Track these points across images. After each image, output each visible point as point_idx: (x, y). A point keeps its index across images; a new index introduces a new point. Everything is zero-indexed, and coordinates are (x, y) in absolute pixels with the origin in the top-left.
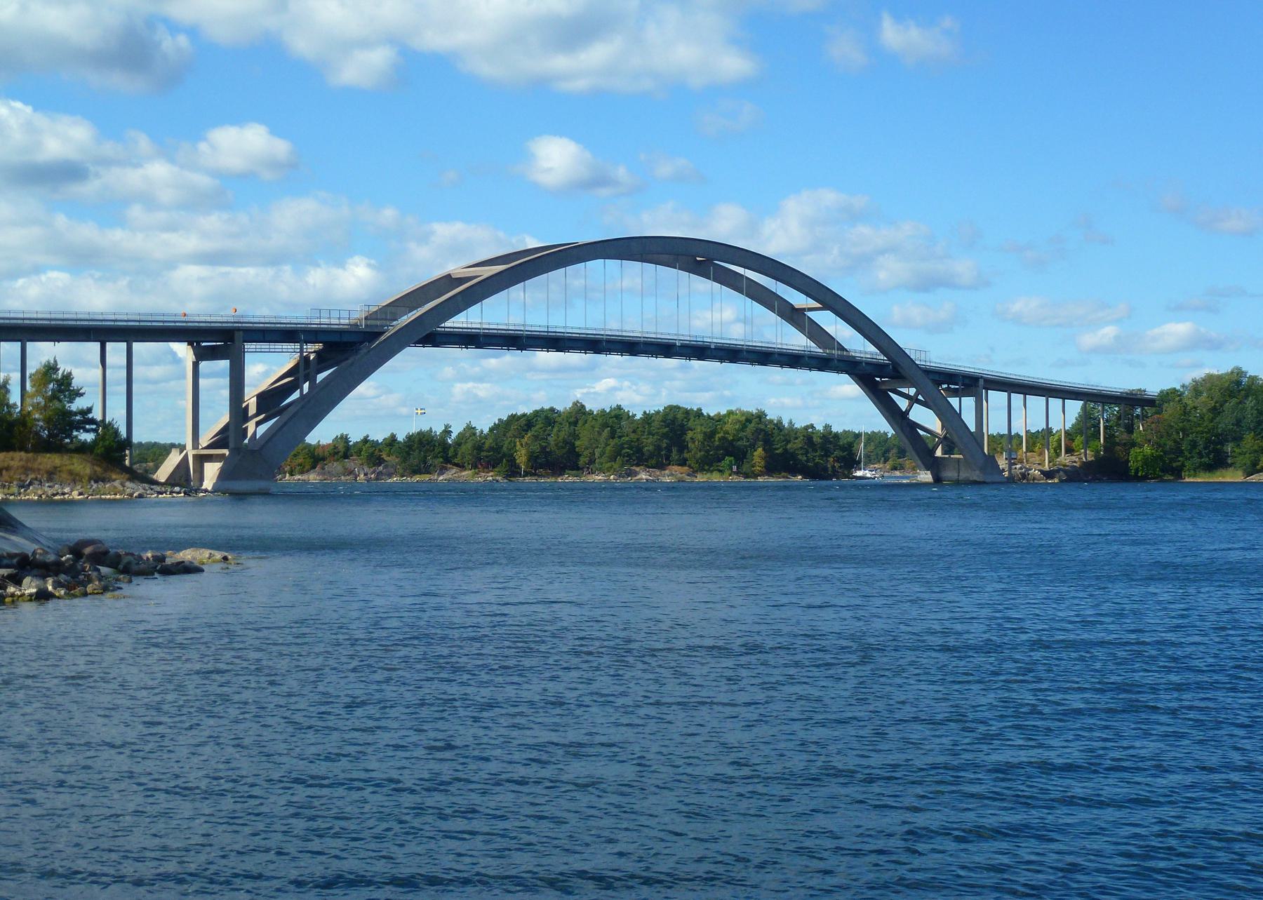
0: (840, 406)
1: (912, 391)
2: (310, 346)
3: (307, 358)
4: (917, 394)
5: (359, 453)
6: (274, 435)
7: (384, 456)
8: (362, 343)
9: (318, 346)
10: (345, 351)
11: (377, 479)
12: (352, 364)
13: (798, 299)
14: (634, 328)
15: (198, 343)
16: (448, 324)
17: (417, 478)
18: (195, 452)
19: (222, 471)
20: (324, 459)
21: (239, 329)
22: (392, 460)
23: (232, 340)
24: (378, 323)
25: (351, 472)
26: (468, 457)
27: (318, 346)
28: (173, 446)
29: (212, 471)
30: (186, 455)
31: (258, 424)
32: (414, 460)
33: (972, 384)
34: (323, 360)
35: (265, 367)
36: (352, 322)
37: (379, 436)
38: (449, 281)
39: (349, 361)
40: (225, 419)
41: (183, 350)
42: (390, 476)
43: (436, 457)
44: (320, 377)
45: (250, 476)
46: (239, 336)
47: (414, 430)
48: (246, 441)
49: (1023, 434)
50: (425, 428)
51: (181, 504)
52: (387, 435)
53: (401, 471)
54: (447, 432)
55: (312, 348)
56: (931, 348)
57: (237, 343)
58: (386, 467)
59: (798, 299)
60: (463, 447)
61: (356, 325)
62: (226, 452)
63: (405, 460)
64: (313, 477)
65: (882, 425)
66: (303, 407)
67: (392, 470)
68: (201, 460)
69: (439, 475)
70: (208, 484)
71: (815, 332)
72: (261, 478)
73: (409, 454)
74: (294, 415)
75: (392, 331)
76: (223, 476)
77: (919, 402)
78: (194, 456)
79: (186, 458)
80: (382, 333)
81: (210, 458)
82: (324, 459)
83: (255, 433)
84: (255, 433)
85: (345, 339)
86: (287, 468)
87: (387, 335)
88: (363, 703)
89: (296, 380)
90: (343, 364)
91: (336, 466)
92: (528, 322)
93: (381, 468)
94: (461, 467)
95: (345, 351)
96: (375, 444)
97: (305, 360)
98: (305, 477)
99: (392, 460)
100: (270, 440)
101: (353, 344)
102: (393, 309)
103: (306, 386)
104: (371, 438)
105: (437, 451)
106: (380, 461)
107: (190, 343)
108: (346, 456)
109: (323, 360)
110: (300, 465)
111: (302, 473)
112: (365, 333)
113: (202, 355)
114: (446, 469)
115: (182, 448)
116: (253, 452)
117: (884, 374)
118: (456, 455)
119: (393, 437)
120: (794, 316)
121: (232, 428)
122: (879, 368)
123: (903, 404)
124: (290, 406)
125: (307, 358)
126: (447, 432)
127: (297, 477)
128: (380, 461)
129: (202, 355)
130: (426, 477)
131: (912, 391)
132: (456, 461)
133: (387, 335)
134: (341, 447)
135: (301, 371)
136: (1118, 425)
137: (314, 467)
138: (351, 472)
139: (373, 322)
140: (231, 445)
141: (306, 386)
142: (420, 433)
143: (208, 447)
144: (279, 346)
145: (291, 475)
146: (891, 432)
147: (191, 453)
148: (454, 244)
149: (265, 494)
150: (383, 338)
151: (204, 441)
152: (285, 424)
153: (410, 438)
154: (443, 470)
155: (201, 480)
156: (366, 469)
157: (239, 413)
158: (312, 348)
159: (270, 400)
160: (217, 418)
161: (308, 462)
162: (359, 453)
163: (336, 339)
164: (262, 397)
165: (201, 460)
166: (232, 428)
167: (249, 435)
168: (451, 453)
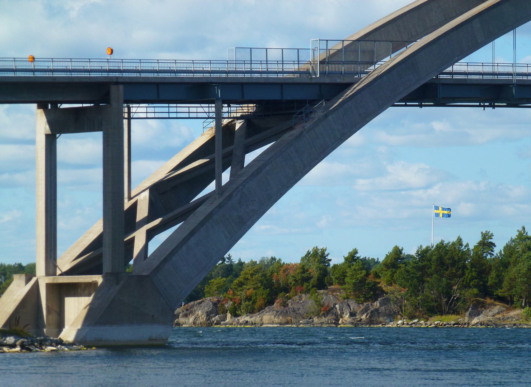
2: (234, 108)
3: (230, 127)
5: (341, 281)
6: (173, 253)
7: (383, 285)
8: (313, 102)
9: (249, 108)
10: (288, 116)
11: (370, 322)
12: (299, 137)
15: (55, 104)
16: (458, 67)
17: (435, 321)
18: (50, 280)
19: (92, 310)
20: (286, 289)
21: (117, 82)
22: (394, 291)
23: (106, 98)
24: (343, 68)
25: (329, 311)
26: (520, 288)
27: (249, 108)
28: (19, 269)
29: (76, 308)
30: (36, 285)
31: (150, 234)
32: (430, 292)
34: (255, 130)
35: (164, 141)
36: (303, 67)
37: (376, 250)
39: (295, 132)
40: (97, 228)
41: (32, 120)
42: (392, 316)
43: (467, 286)
44: (250, 158)
45: (138, 317)
46: (117, 92)
47: (431, 240)
48: (131, 262)
50: (450, 238)
51: (343, 344)
52: (389, 249)
53: (409, 309)
54: (486, 243)
55: (236, 113)
57: (114, 104)
58: (386, 301)
60: (513, 271)
61: (307, 72)
62: (99, 279)
63: (416, 291)
64: (268, 319)
66: (220, 206)
67: (394, 307)
68: (60, 292)
69: (472, 316)
70: (68, 334)
72: (153, 321)
73: (421, 281)
74: (210, 216)
75: (365, 80)
76: (92, 318)
78: (49, 286)
79: (36, 287)
80: (349, 85)
81: (73, 290)
82: (286, 289)
83: (146, 247)
84: (145, 248)
85: (290, 95)
86: (229, 305)
87: (357, 87)
89: (211, 162)
90: (287, 136)
91: (306, 301)
92: (521, 60)
93: (377, 304)
94: (508, 302)
95: (288, 116)
96: (367, 265)
97: (225, 133)
98: (255, 318)
99: (394, 291)
100: (165, 260)
101: (301, 103)
102: (368, 46)
103: (226, 176)
104: (361, 255)
105: (468, 275)
106: (375, 292)
107: (42, 105)
108: (321, 284)
109: (255, 130)
110: (248, 298)
111: (251, 311)
112: (320, 85)
113: (62, 124)
114: (484, 306)
115: (28, 272)
116: (141, 279)
118: (499, 284)
119: (397, 252)
121: (107, 241)
124: (204, 202)
125: (230, 127)
126: (486, 243)
127: (243, 319)
128: (375, 292)
129: (62, 124)
130: (451, 319)
132: (499, 292)
133: (357, 87)
134: (314, 271)
135: (222, 148)
137: (270, 302)
138: (329, 311)
139: (333, 68)
140: (107, 267)
141: (226, 176)
142: (441, 247)
143: (71, 272)
144: (183, 108)
145: (235, 315)
147: (43, 280)
149: (160, 346)
150: (349, 93)
151: (66, 260)
152: (192, 234)
153: (424, 254)
154: (478, 308)
155: (60, 325)
156: (353, 305)
157: (119, 219)
158: (236, 113)
159: (170, 196)
160: (83, 224)
161: (262, 295)
162: (341, 281)
163: (274, 95)
164: (157, 190)
165: (60, 292)
166: (107, 241)
167: (136, 251)
168: (491, 279)
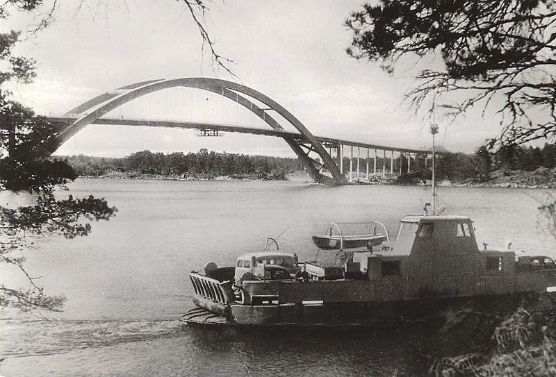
0: (280, 150)
1: (310, 145)
4: (312, 147)
13: (261, 106)
14: (148, 118)
33: (335, 144)
38: (107, 96)
49: (350, 158)
56: (315, 130)
59: (261, 106)
65: (294, 156)
71: (269, 120)
77: (313, 150)
80: (76, 119)
88: (434, 98)
117: (297, 140)
120: (260, 113)
122: (296, 136)
123: (306, 151)
131: (310, 145)
136: (434, 281)
146: (297, 157)
148: (114, 80)
